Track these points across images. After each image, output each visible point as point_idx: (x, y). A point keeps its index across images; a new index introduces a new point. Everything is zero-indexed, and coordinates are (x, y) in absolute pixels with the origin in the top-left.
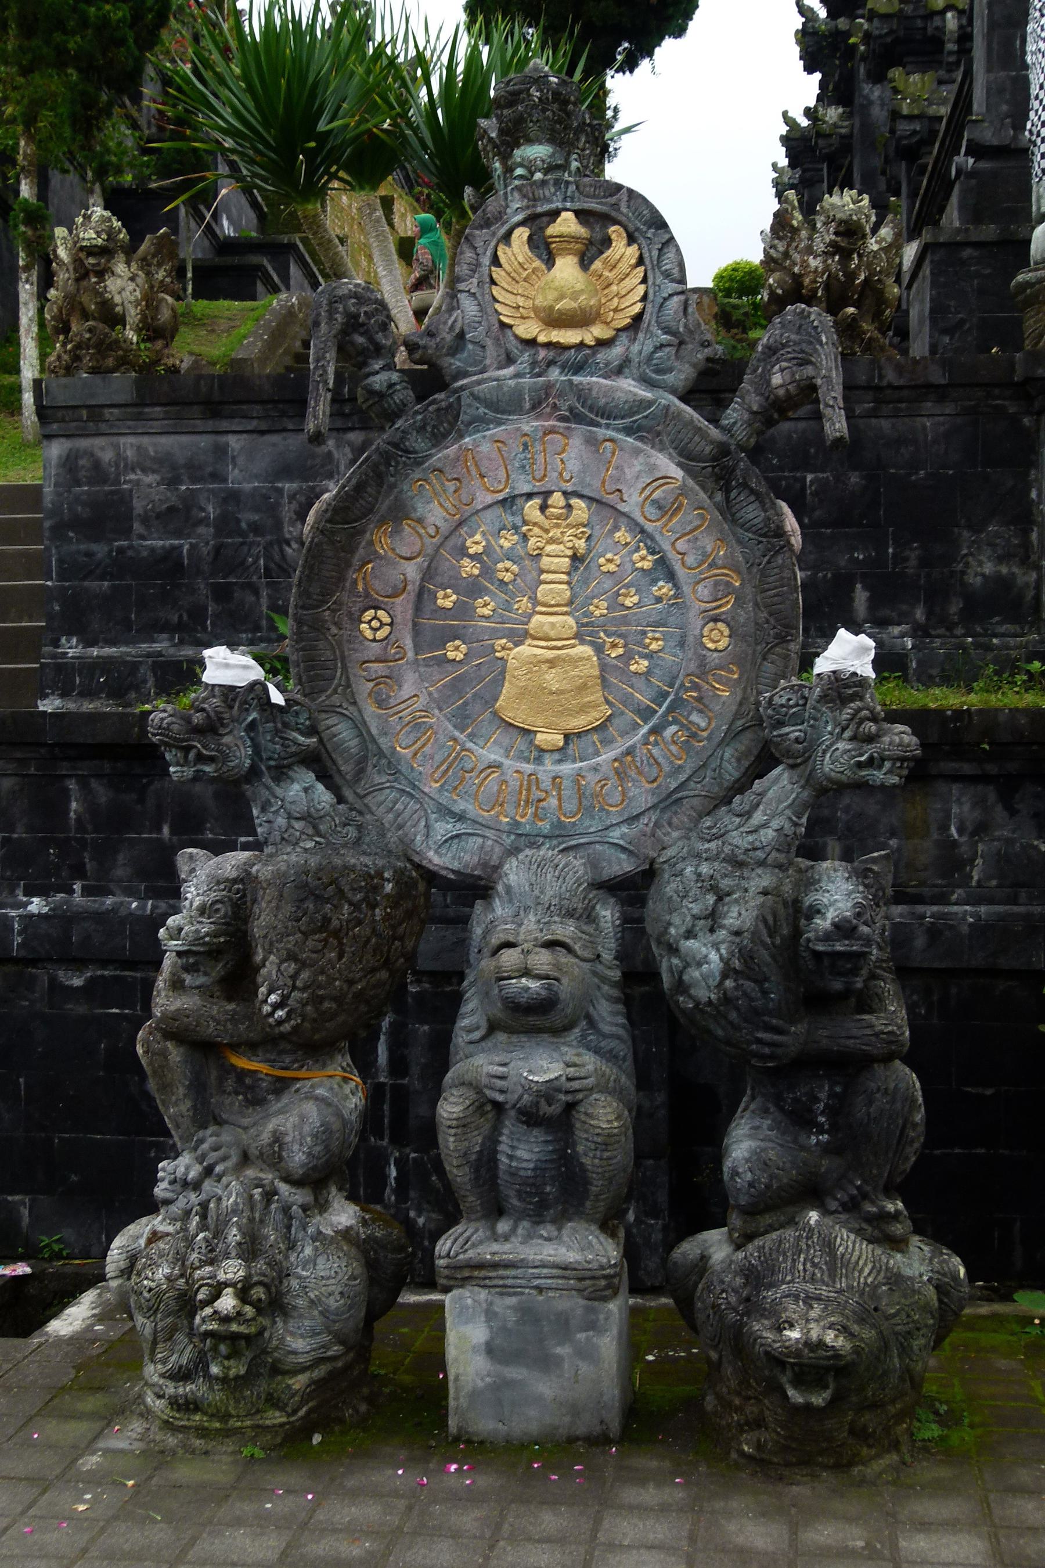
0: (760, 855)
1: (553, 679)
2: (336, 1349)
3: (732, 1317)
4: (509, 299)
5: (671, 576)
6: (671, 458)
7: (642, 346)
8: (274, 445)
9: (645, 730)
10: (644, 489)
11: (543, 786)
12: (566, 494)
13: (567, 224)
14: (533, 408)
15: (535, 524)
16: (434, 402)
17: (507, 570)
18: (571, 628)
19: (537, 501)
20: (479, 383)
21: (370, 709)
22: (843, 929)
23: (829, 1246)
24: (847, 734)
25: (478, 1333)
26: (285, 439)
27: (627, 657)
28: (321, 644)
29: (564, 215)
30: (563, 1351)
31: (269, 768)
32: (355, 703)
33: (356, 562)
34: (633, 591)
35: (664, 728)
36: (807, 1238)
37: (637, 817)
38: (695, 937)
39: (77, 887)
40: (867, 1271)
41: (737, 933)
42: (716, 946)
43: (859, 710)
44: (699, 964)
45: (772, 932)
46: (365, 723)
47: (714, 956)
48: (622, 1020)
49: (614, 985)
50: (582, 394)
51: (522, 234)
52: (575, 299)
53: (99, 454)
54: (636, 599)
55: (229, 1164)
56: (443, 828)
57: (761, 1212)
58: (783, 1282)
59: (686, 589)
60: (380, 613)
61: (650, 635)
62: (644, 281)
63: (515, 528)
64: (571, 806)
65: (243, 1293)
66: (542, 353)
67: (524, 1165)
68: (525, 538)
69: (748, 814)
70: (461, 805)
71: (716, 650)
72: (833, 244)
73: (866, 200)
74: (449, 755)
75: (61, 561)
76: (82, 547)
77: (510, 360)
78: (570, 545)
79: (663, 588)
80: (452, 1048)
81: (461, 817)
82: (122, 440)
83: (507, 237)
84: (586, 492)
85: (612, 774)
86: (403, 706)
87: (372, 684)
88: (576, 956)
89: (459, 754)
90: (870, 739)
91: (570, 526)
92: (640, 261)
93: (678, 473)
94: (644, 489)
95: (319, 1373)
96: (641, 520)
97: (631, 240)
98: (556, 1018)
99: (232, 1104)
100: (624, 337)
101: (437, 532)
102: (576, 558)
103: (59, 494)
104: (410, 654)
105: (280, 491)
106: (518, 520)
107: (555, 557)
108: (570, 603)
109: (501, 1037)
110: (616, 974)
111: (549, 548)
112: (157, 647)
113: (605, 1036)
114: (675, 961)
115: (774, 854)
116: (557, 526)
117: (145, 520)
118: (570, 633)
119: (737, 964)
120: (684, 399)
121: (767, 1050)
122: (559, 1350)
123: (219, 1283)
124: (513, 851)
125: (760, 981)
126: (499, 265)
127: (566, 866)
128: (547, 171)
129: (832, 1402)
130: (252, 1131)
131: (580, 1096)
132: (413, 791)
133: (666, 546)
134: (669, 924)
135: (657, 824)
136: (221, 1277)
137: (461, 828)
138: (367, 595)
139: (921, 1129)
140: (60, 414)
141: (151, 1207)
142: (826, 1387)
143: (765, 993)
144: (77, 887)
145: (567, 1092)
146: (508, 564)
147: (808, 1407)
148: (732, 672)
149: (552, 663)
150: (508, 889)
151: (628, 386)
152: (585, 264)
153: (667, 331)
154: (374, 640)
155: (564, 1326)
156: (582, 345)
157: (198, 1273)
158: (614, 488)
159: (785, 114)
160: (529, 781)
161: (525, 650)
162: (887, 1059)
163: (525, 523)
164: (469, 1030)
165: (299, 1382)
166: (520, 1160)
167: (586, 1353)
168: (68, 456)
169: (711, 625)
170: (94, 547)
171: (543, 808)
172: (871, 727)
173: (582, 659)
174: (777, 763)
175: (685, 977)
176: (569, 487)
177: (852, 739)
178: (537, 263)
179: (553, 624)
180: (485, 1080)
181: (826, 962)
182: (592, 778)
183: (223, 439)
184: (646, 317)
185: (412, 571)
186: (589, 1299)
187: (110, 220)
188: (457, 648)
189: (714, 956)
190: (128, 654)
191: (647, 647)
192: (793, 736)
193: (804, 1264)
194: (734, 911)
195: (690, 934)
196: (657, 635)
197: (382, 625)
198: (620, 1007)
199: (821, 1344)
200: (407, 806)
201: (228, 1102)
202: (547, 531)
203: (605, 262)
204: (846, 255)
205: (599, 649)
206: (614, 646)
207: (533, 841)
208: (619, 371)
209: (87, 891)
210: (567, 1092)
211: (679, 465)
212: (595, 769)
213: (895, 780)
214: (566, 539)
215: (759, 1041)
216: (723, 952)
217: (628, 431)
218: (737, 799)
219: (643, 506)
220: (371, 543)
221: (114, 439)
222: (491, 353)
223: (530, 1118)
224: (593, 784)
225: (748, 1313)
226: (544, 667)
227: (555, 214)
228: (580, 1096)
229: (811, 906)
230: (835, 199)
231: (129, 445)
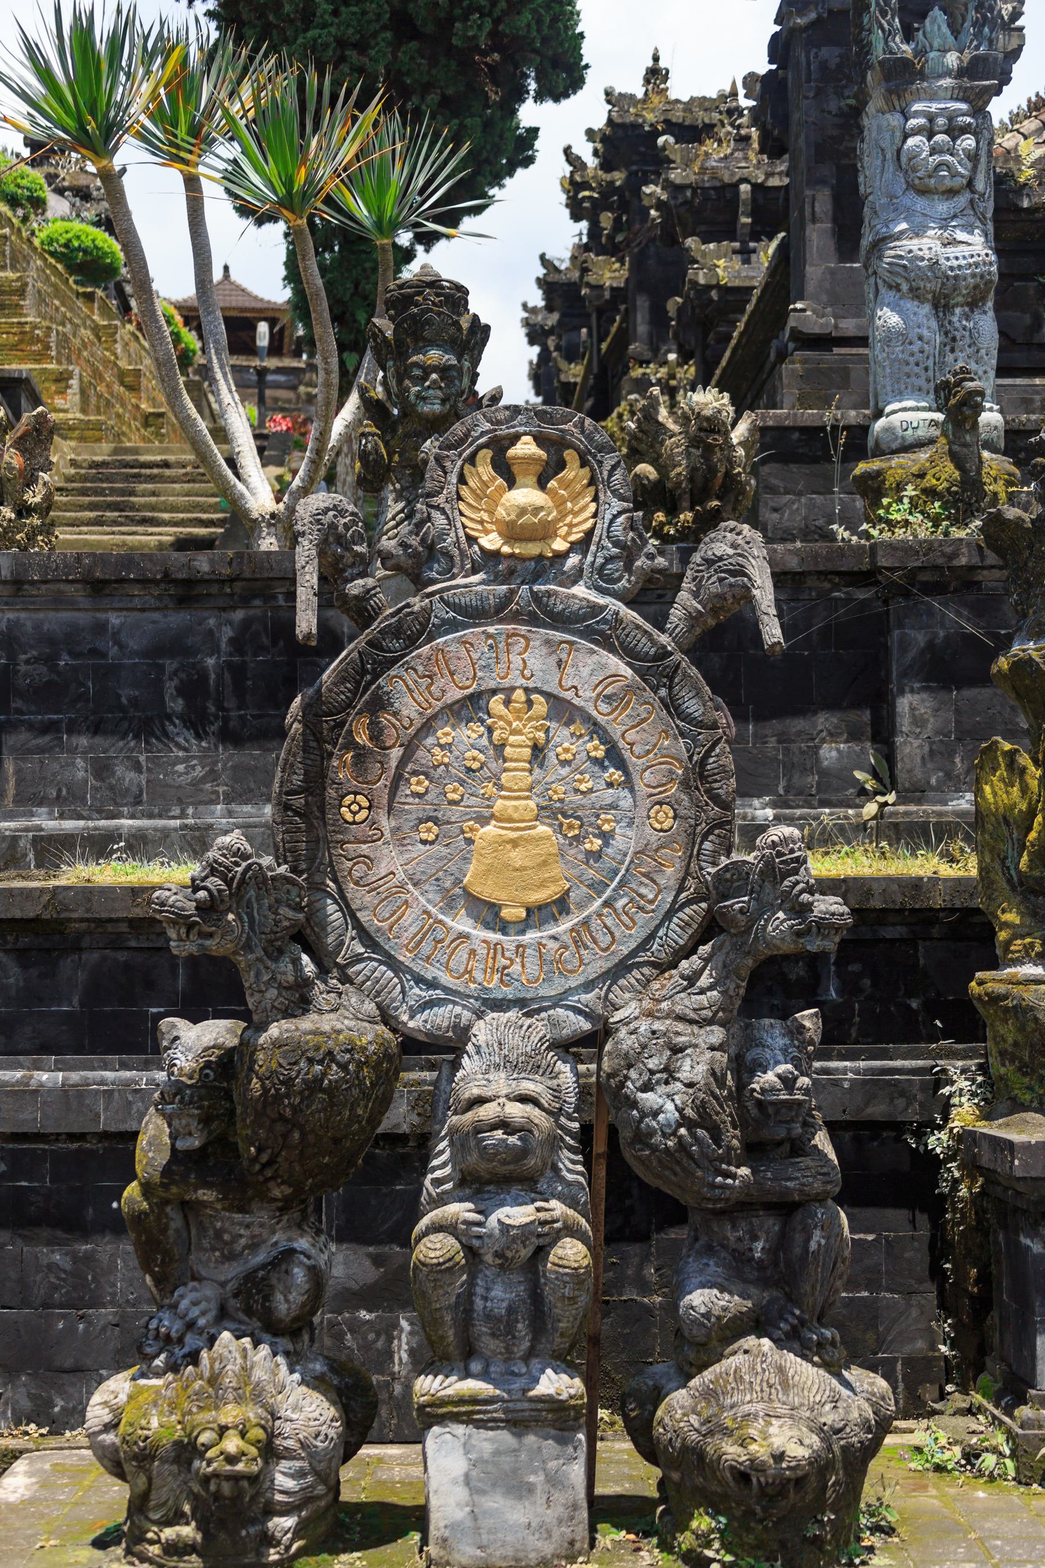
0: (708, 1013)
6: (621, 658)
8: (154, 622)
10: (597, 686)
11: (507, 954)
12: (527, 690)
15: (501, 718)
16: (408, 606)
17: (474, 759)
18: (532, 810)
19: (501, 696)
23: (781, 1370)
26: (165, 616)
34: (587, 776)
35: (615, 900)
36: (762, 1362)
38: (652, 1090)
40: (814, 1391)
41: (690, 1085)
42: (670, 1096)
45: (721, 1082)
47: (669, 1106)
51: (486, 454)
54: (590, 785)
56: (417, 992)
60: (359, 797)
61: (602, 816)
68: (490, 730)
71: (661, 830)
74: (423, 927)
78: (531, 735)
83: (472, 460)
84: (545, 688)
85: (570, 942)
86: (381, 882)
88: (543, 1109)
89: (431, 926)
93: (628, 672)
94: (597, 686)
99: (209, 1260)
101: (411, 725)
111: (512, 739)
112: (36, 821)
118: (531, 815)
119: (689, 1112)
120: (628, 604)
122: (532, 1479)
124: (480, 1015)
126: (466, 483)
127: (529, 1027)
133: (616, 736)
134: (627, 1078)
136: (223, 1420)
137: (439, 993)
146: (476, 753)
148: (677, 851)
149: (515, 843)
153: (616, 544)
154: (354, 823)
158: (570, 684)
160: (495, 950)
161: (491, 830)
162: (820, 1199)
169: (657, 807)
171: (507, 975)
173: (541, 838)
176: (531, 684)
178: (500, 481)
179: (516, 808)
184: (597, 532)
186: (561, 1430)
189: (669, 1106)
191: (599, 827)
192: (737, 906)
193: (761, 1385)
194: (687, 1064)
195: (647, 1088)
196: (609, 817)
197: (361, 808)
201: (204, 1259)
203: (560, 482)
206: (571, 827)
207: (500, 1005)
211: (628, 664)
214: (527, 730)
216: (678, 1102)
218: (684, 964)
219: (596, 701)
220: (350, 732)
224: (552, 952)
226: (509, 847)
227: (515, 438)
229: (754, 1060)
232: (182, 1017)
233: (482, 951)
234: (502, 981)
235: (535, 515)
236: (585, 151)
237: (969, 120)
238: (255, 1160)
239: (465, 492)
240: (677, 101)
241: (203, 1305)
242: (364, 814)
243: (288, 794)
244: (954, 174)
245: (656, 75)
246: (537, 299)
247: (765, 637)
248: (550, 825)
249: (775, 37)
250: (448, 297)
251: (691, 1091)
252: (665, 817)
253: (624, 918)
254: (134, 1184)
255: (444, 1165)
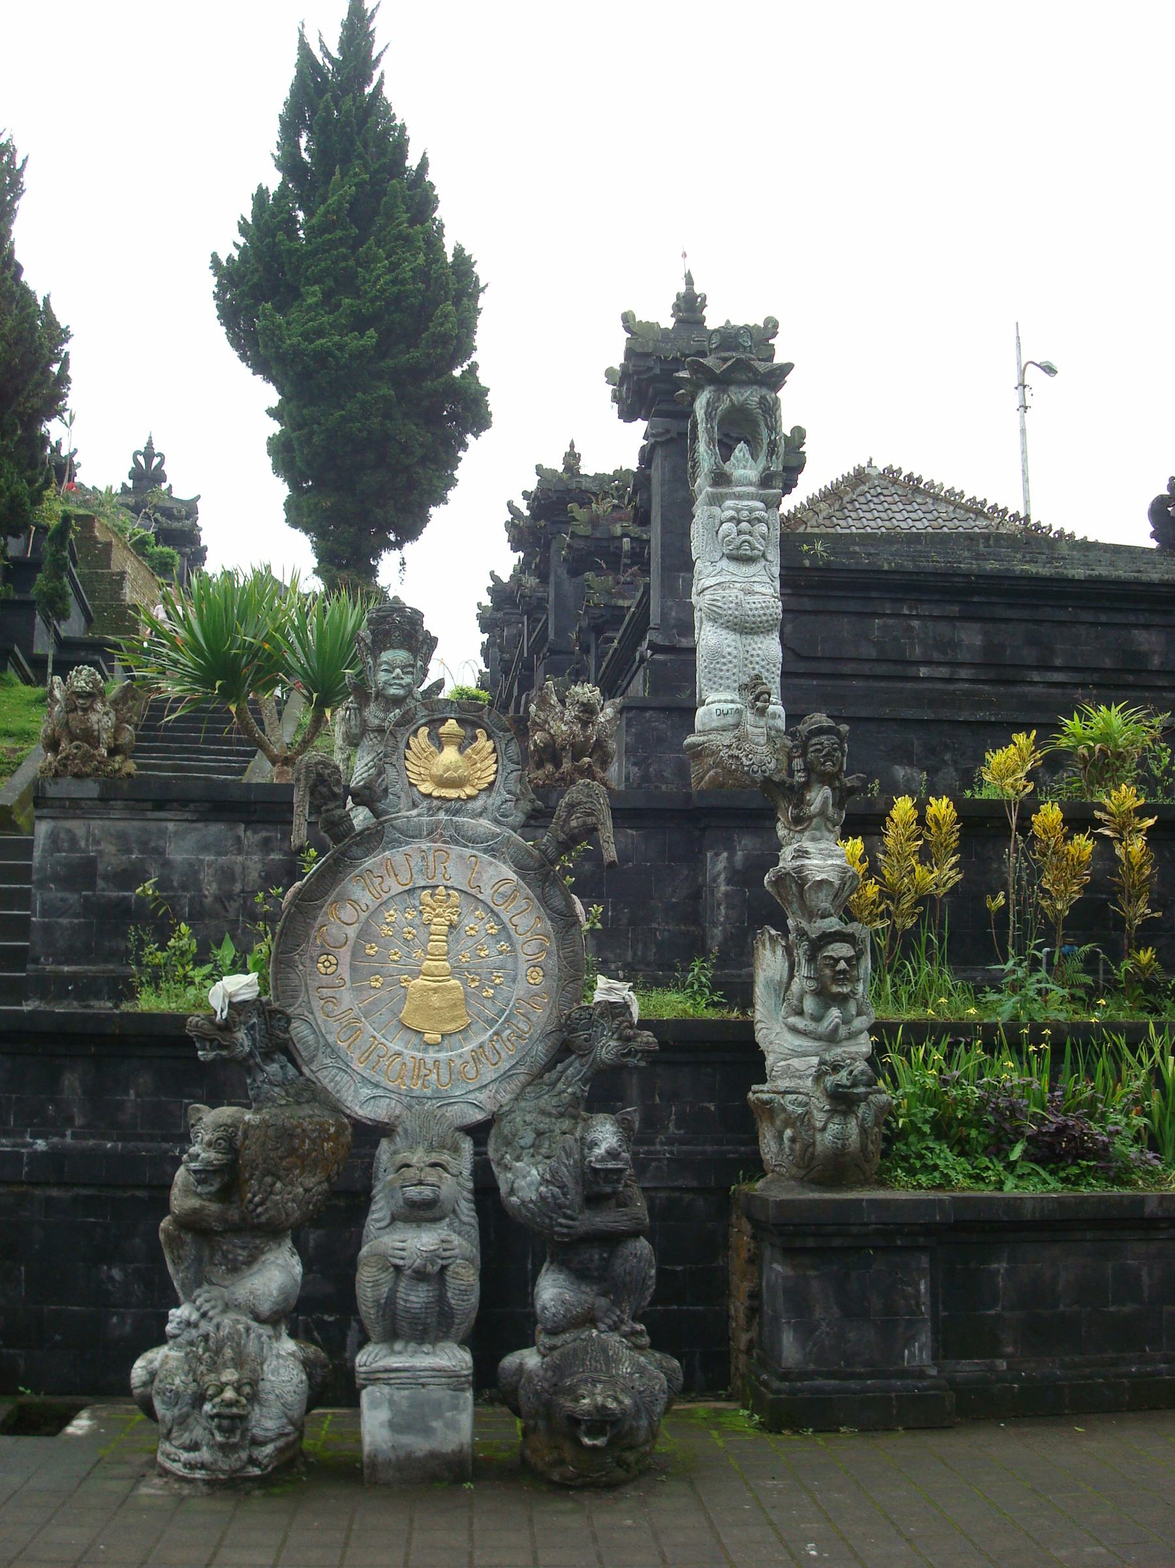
1: (435, 999)
2: (290, 1428)
3: (546, 1396)
4: (416, 769)
5: (509, 939)
6: (510, 867)
7: (495, 800)
9: (491, 1032)
12: (446, 887)
13: (451, 726)
14: (428, 835)
20: (396, 819)
21: (320, 1016)
22: (612, 1154)
24: (615, 1036)
25: (384, 1414)
27: (481, 988)
28: (292, 976)
29: (450, 721)
30: (436, 1424)
31: (260, 1053)
32: (312, 1013)
33: (317, 925)
37: (485, 1086)
39: (69, 1133)
43: (621, 1023)
44: (524, 1177)
46: (317, 1024)
48: (474, 1214)
49: (470, 1191)
50: (458, 828)
51: (424, 731)
52: (456, 771)
53: (77, 831)
54: (487, 952)
55: (217, 1310)
56: (366, 1092)
57: (564, 1331)
58: (578, 1373)
59: (518, 947)
62: (496, 762)
63: (415, 907)
64: (445, 1079)
65: (238, 1390)
66: (435, 802)
67: (415, 1305)
69: (554, 1084)
70: (377, 1078)
72: (576, 717)
73: (598, 691)
75: (43, 903)
76: (60, 895)
77: (415, 805)
79: (504, 946)
80: (364, 1232)
81: (377, 1086)
82: (92, 822)
83: (415, 733)
85: (470, 1059)
87: (322, 1002)
90: (629, 1039)
91: (448, 907)
92: (494, 750)
93: (515, 877)
95: (280, 1443)
96: (492, 905)
97: (489, 738)
98: (436, 1212)
100: (483, 796)
102: (452, 926)
103: (44, 857)
104: (348, 984)
105: (201, 861)
106: (417, 904)
107: (439, 926)
108: (447, 954)
109: (400, 1224)
110: (470, 1185)
111: (435, 920)
113: (465, 1224)
114: (509, 1175)
115: (570, 1109)
116: (441, 907)
117: (105, 877)
119: (548, 1177)
121: (565, 1230)
123: (222, 1383)
125: (562, 1187)
128: (402, 668)
129: (610, 1443)
130: (231, 1288)
131: (450, 1261)
132: (346, 1069)
133: (506, 921)
135: (496, 1092)
136: (224, 1379)
137: (380, 1092)
138: (322, 946)
139: (654, 1280)
140: (49, 803)
141: (161, 1339)
142: (605, 1435)
143: (565, 1194)
144: (69, 1133)
145: (443, 1259)
147: (594, 1446)
149: (435, 990)
150: (406, 1131)
151: (485, 824)
152: (461, 749)
153: (509, 792)
155: (437, 1409)
156: (459, 798)
157: (207, 1378)
159: (492, 574)
161: (419, 982)
163: (421, 904)
164: (377, 1221)
165: (269, 1449)
166: (411, 1302)
167: (453, 1425)
168: (52, 832)
170: (67, 895)
172: (630, 1032)
173: (453, 988)
174: (572, 1052)
175: (515, 1185)
176: (449, 883)
177: (618, 1039)
178: (433, 749)
180: (391, 1252)
181: (602, 1175)
182: (458, 1062)
183: (164, 824)
185: (352, 932)
187: (94, 674)
188: (377, 980)
190: (89, 971)
191: (493, 981)
198: (472, 1206)
199: (604, 1407)
200: (343, 1078)
202: (434, 910)
204: (585, 724)
205: (465, 983)
206: (473, 980)
208: (480, 815)
209: (75, 1136)
210: (443, 1259)
211: (515, 872)
212: (460, 1056)
213: (643, 1064)
215: (561, 1225)
217: (485, 851)
218: (547, 1076)
221: (86, 822)
222: (404, 802)
223: (420, 1276)
225: (555, 1393)
226: (431, 993)
227: (444, 721)
228: (450, 1261)
230: (578, 689)
231: (96, 825)
232: (204, 1104)
233: (410, 1065)
234: (423, 1084)
235: (456, 771)
236: (522, 505)
237: (763, 513)
238: (251, 1201)
239: (409, 753)
240: (586, 475)
241: (212, 1303)
242: (323, 970)
243: (282, 953)
244: (753, 549)
245: (572, 459)
246: (487, 601)
247: (605, 857)
248: (459, 979)
249: (643, 448)
250: (408, 617)
251: (548, 1161)
252: (537, 977)
253: (508, 1044)
254: (168, 1217)
255: (381, 1209)
